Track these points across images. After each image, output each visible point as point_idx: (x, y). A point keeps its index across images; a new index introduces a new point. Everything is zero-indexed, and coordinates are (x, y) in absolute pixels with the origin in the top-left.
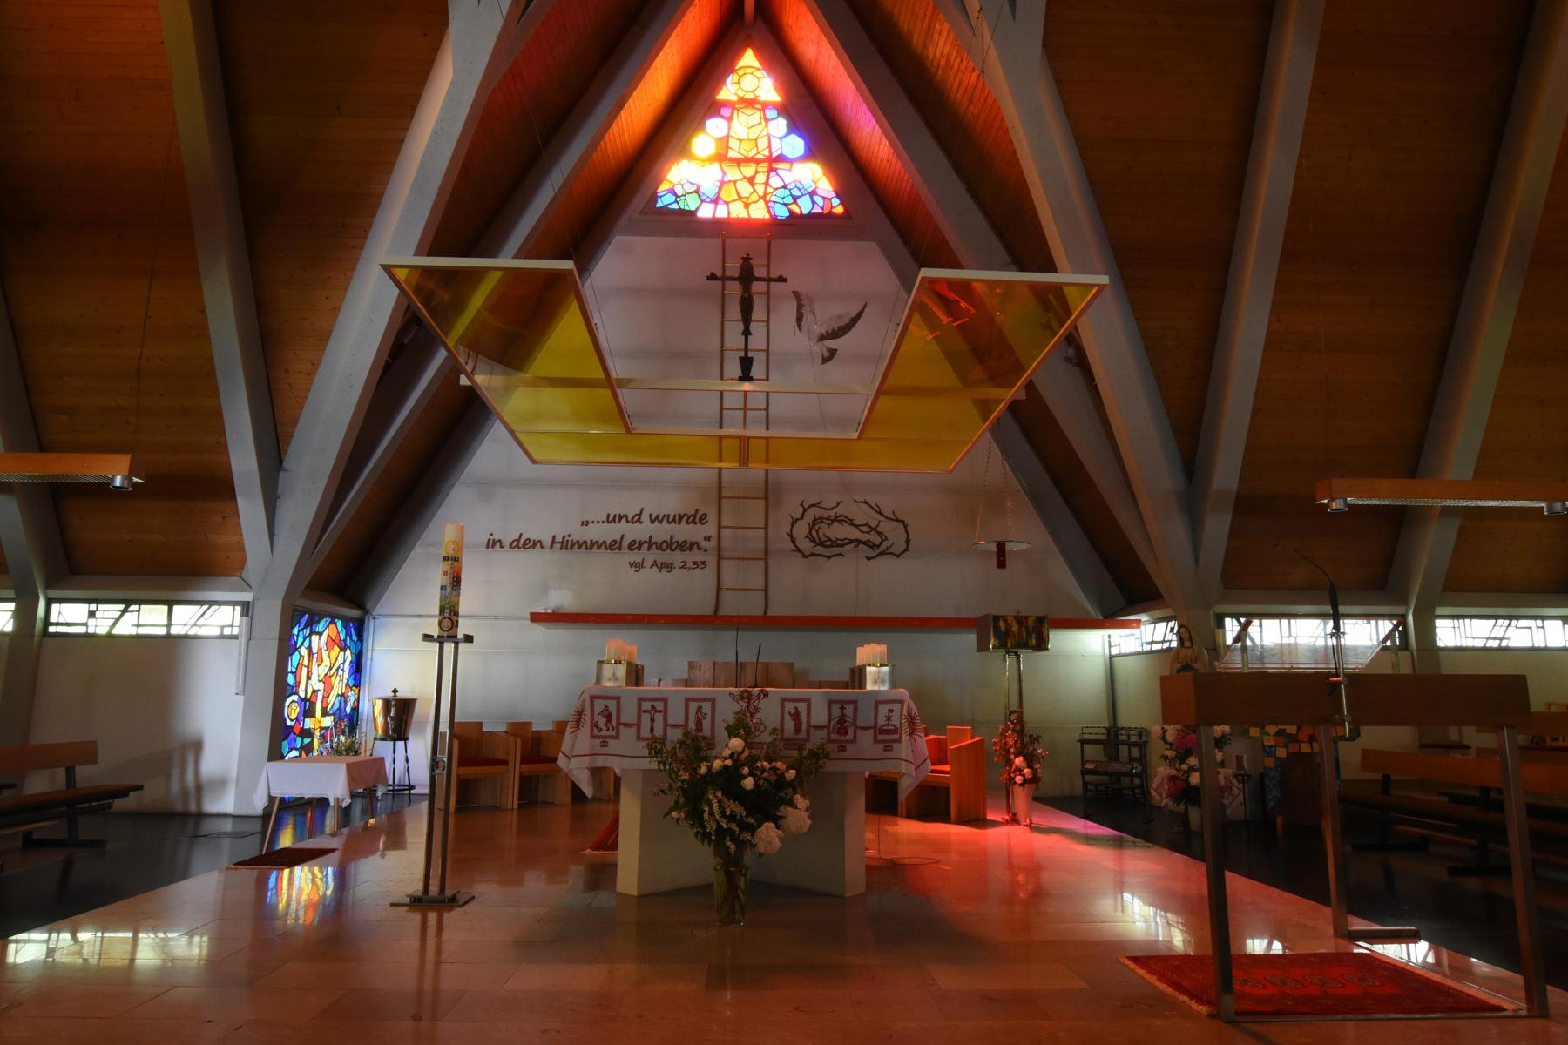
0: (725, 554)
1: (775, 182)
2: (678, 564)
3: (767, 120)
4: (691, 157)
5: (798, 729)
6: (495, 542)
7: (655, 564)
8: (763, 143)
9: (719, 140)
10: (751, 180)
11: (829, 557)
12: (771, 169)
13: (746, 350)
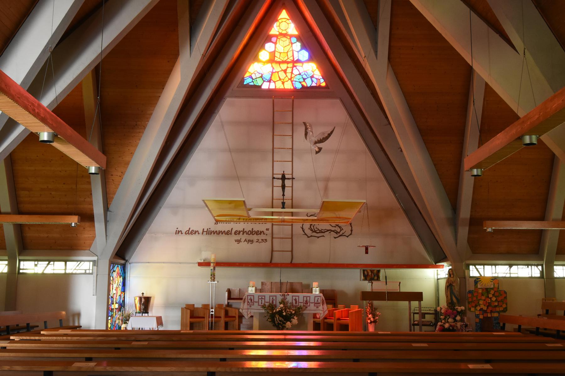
0: (274, 236)
3: (292, 44)
4: (259, 61)
5: (296, 303)
6: (179, 232)
7: (245, 240)
8: (290, 54)
9: (271, 53)
10: (285, 71)
11: (318, 237)
12: (294, 66)
13: (283, 199)
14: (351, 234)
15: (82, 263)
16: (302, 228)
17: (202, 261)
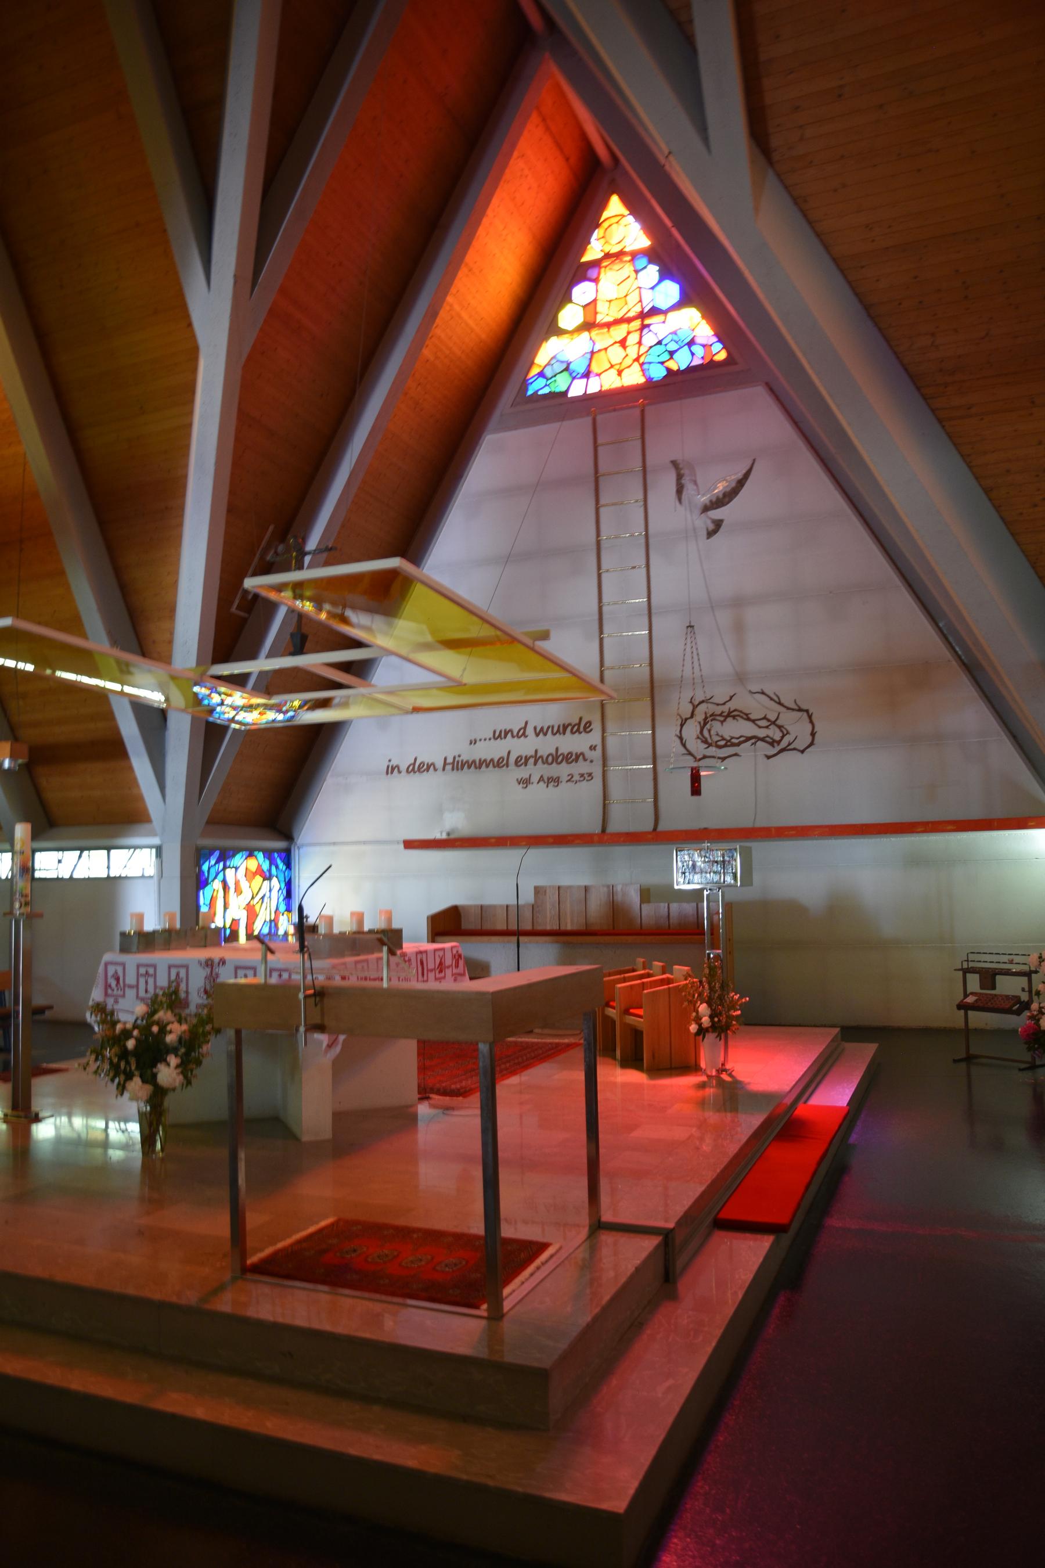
1: (649, 339)
2: (564, 778)
4: (560, 332)
8: (633, 298)
10: (623, 343)
11: (723, 759)
12: (644, 327)
14: (812, 744)
15: (138, 851)
16: (681, 738)
17: (444, 836)
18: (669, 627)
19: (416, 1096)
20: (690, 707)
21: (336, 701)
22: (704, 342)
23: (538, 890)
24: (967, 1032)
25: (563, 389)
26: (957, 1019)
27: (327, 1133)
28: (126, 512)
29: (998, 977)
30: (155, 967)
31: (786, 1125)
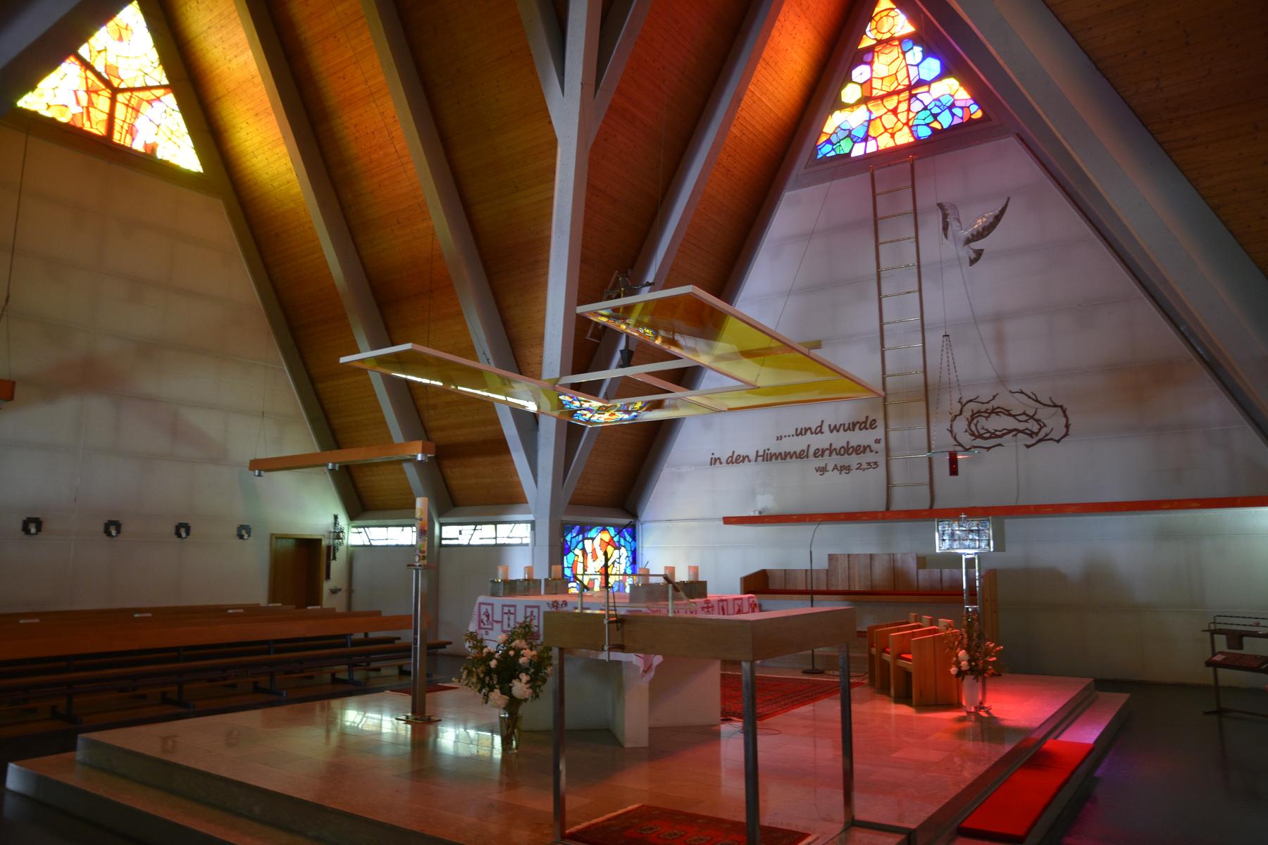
1: (916, 106)
2: (855, 466)
3: (904, 53)
4: (842, 106)
7: (835, 467)
8: (902, 75)
10: (894, 111)
11: (988, 449)
12: (912, 96)
14: (1066, 435)
18: (934, 339)
19: (718, 716)
20: (959, 406)
21: (667, 403)
22: (963, 104)
23: (832, 558)
24: (1216, 689)
25: (847, 151)
26: (1207, 676)
27: (644, 742)
28: (505, 265)
29: (1245, 639)
30: (514, 606)
31: (1032, 754)
